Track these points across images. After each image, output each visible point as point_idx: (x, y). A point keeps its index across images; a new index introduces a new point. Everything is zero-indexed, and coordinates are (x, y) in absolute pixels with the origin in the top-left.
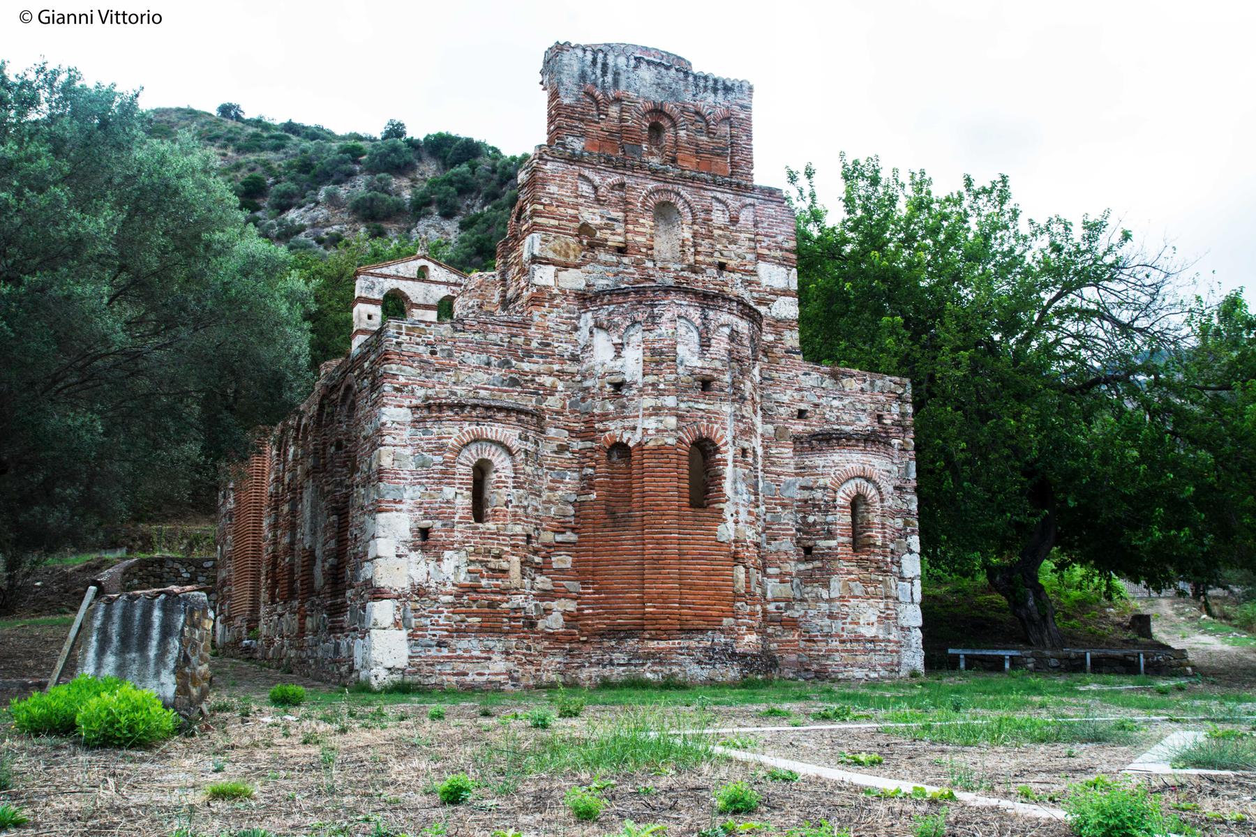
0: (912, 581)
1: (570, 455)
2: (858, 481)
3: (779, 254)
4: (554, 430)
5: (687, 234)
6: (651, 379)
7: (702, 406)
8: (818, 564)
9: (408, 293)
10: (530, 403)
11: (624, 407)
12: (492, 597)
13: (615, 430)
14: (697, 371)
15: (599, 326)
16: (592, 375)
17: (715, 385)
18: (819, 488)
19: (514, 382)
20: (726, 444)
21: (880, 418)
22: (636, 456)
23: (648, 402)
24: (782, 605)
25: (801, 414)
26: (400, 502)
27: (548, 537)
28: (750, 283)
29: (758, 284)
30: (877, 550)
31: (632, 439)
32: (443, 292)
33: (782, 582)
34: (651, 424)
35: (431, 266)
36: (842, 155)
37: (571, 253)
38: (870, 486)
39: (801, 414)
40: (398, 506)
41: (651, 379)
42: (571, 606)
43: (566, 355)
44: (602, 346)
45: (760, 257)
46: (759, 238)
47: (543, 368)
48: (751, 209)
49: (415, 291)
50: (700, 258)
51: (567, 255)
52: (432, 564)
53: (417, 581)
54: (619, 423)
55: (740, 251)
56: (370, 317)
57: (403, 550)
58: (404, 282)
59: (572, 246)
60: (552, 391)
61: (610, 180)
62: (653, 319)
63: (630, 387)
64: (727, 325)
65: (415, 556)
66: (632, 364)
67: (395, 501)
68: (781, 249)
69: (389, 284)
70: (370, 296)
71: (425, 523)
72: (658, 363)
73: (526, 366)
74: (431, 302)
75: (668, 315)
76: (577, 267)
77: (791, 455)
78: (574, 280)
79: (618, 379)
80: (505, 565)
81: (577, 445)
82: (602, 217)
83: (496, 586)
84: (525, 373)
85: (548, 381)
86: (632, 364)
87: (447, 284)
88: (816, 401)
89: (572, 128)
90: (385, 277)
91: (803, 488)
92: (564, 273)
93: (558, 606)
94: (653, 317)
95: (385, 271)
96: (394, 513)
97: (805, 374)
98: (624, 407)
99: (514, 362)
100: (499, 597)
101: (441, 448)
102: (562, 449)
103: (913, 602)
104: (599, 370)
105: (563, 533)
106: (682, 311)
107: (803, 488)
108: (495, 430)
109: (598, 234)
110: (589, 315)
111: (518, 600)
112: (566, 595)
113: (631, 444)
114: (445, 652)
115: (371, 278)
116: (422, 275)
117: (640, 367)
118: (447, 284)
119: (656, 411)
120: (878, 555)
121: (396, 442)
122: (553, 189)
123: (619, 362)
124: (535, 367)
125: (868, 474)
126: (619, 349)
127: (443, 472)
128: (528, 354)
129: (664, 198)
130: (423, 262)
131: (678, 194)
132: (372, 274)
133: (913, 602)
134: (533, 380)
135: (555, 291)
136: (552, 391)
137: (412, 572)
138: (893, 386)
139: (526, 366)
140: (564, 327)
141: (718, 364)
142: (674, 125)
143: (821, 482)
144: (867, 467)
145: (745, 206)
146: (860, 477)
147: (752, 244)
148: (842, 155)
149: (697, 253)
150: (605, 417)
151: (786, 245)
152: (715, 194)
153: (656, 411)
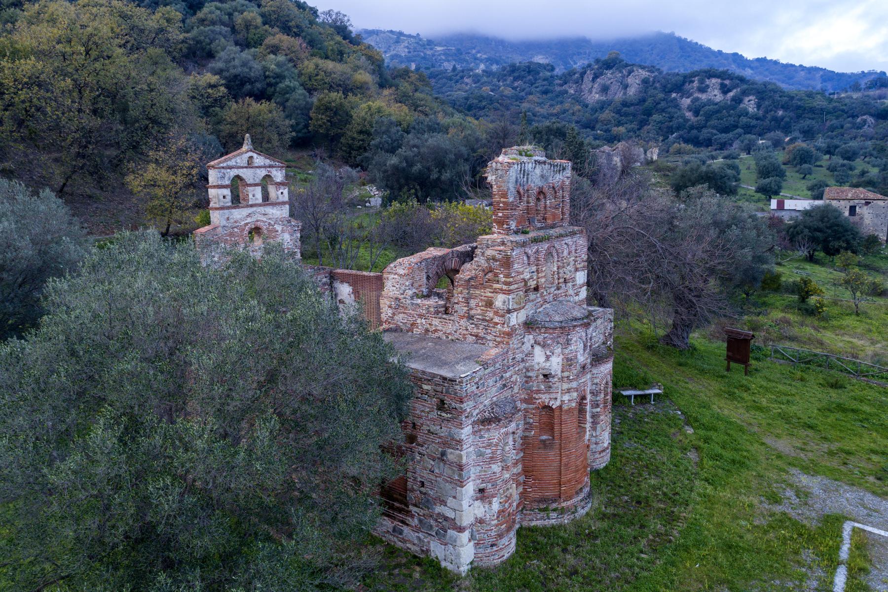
6: (566, 374)
9: (244, 176)
11: (550, 387)
13: (545, 398)
15: (537, 343)
16: (533, 370)
22: (557, 413)
23: (565, 386)
31: (555, 404)
32: (263, 173)
34: (566, 398)
35: (255, 155)
41: (566, 374)
44: (539, 355)
49: (247, 175)
52: (487, 506)
53: (479, 516)
54: (547, 396)
56: (224, 197)
58: (241, 170)
62: (568, 342)
63: (553, 377)
65: (478, 503)
66: (555, 364)
69: (233, 173)
70: (224, 183)
71: (483, 486)
72: (570, 365)
74: (258, 181)
75: (574, 339)
79: (545, 372)
86: (555, 364)
87: (265, 167)
90: (231, 168)
94: (568, 340)
95: (230, 163)
98: (550, 387)
101: (489, 445)
104: (537, 367)
110: (531, 337)
113: (554, 407)
114: (495, 548)
115: (223, 170)
116: (250, 164)
117: (560, 367)
118: (265, 167)
119: (569, 391)
123: (548, 364)
126: (548, 358)
127: (491, 458)
130: (250, 154)
132: (223, 168)
137: (476, 512)
142: (545, 198)
150: (538, 391)
153: (569, 391)
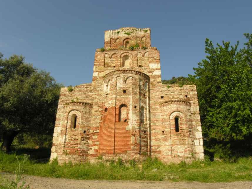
0: (199, 139)
1: (99, 112)
2: (176, 112)
3: (155, 61)
4: (95, 107)
5: (131, 61)
7: (124, 96)
8: (165, 135)
10: (90, 102)
12: (73, 145)
14: (122, 88)
17: (127, 91)
18: (165, 115)
19: (87, 97)
20: (130, 105)
21: (186, 96)
24: (157, 147)
25: (162, 97)
26: (59, 125)
27: (91, 131)
28: (147, 68)
29: (149, 68)
30: (184, 131)
33: (156, 141)
36: (223, 41)
37: (102, 69)
38: (181, 113)
39: (162, 97)
40: (59, 126)
42: (96, 148)
43: (99, 90)
45: (150, 62)
46: (150, 58)
47: (94, 94)
48: (148, 52)
50: (134, 65)
51: (101, 69)
55: (145, 62)
57: (59, 135)
59: (102, 67)
60: (95, 98)
61: (112, 53)
64: (131, 77)
67: (58, 125)
68: (156, 60)
73: (90, 94)
76: (103, 71)
77: (159, 108)
78: (102, 74)
80: (77, 138)
81: (100, 110)
82: (110, 61)
83: (75, 143)
84: (89, 95)
85: (95, 96)
88: (166, 94)
89: (107, 46)
91: (162, 116)
92: (100, 73)
93: (94, 148)
96: (58, 127)
97: (163, 87)
99: (87, 93)
100: (75, 145)
102: (97, 111)
103: (200, 145)
105: (97, 130)
106: (118, 75)
107: (162, 116)
108: (76, 107)
109: (109, 64)
111: (80, 146)
112: (95, 145)
120: (184, 132)
121: (60, 112)
122: (99, 57)
124: (92, 94)
125: (179, 110)
128: (91, 91)
129: (125, 54)
131: (129, 53)
133: (200, 145)
134: (91, 96)
135: (98, 77)
136: (95, 98)
138: (190, 87)
139: (90, 94)
140: (99, 84)
141: (128, 86)
143: (166, 113)
144: (178, 108)
145: (146, 52)
146: (177, 111)
147: (148, 60)
148: (223, 41)
149: (133, 64)
151: (157, 59)
152: (138, 51)
